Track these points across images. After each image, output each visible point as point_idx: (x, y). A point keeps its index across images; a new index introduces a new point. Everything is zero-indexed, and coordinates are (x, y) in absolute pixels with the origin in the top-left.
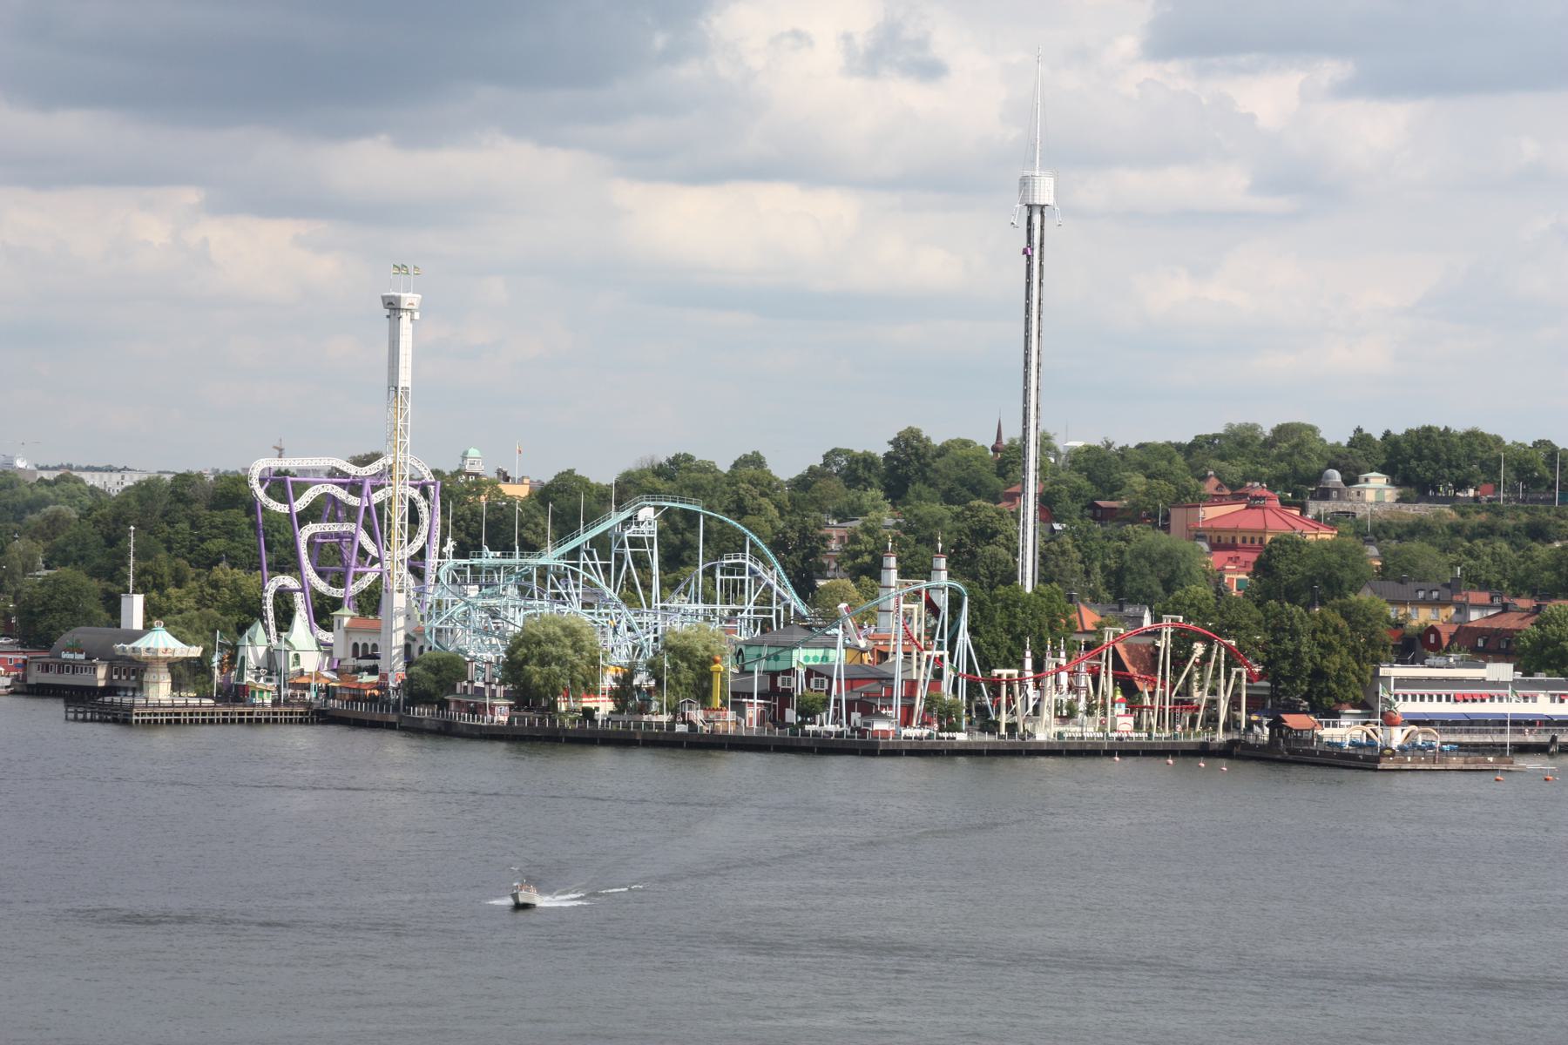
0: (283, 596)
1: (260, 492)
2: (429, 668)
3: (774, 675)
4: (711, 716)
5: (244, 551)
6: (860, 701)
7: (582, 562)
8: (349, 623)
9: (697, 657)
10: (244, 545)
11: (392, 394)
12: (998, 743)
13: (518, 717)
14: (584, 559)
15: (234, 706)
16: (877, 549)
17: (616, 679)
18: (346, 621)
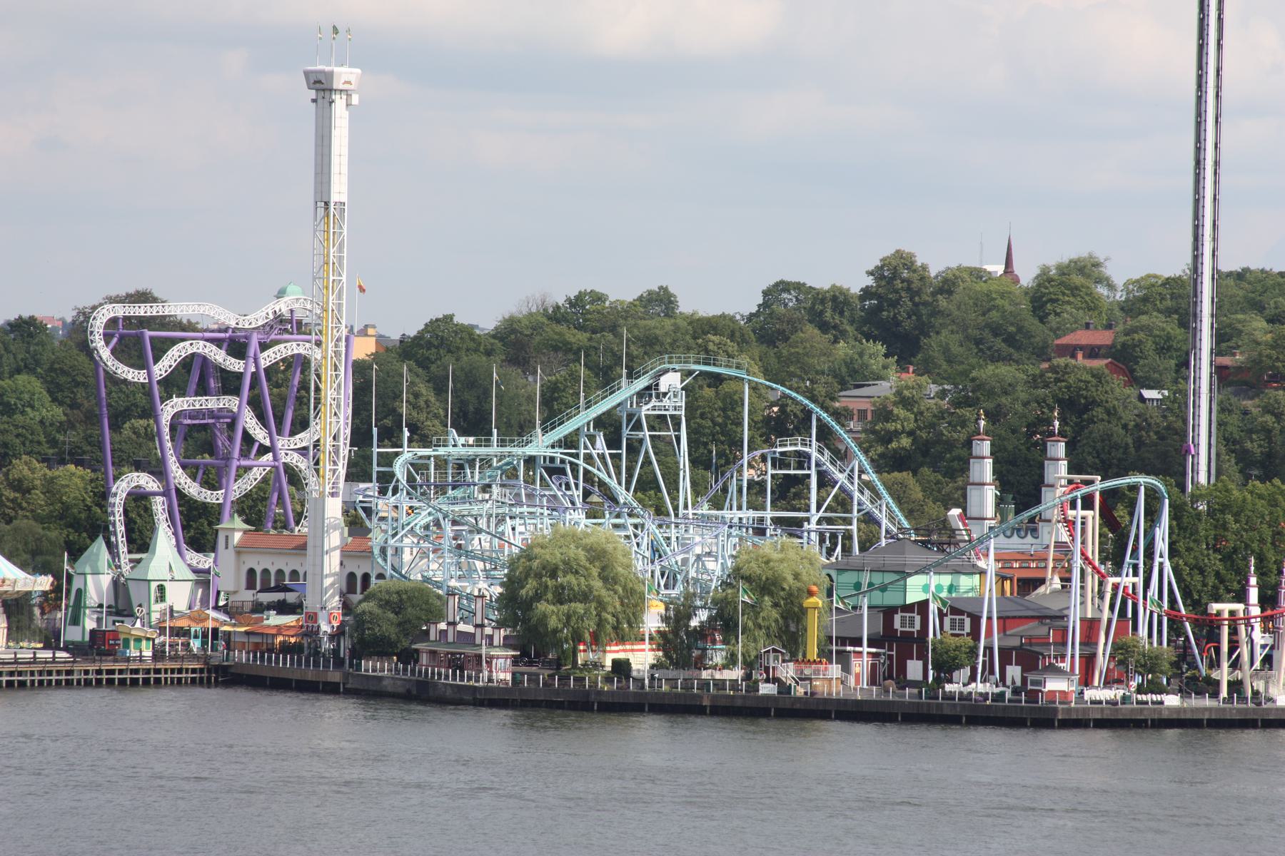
0: (139, 499)
1: (105, 353)
2: (386, 604)
3: (889, 612)
4: (807, 672)
5: (18, 436)
6: (1019, 649)
7: (583, 451)
8: (241, 540)
9: (783, 589)
10: (16, 427)
11: (321, 212)
12: (1224, 709)
13: (529, 674)
14: (586, 447)
15: (101, 661)
16: (919, 428)
17: (665, 619)
18: (237, 536)
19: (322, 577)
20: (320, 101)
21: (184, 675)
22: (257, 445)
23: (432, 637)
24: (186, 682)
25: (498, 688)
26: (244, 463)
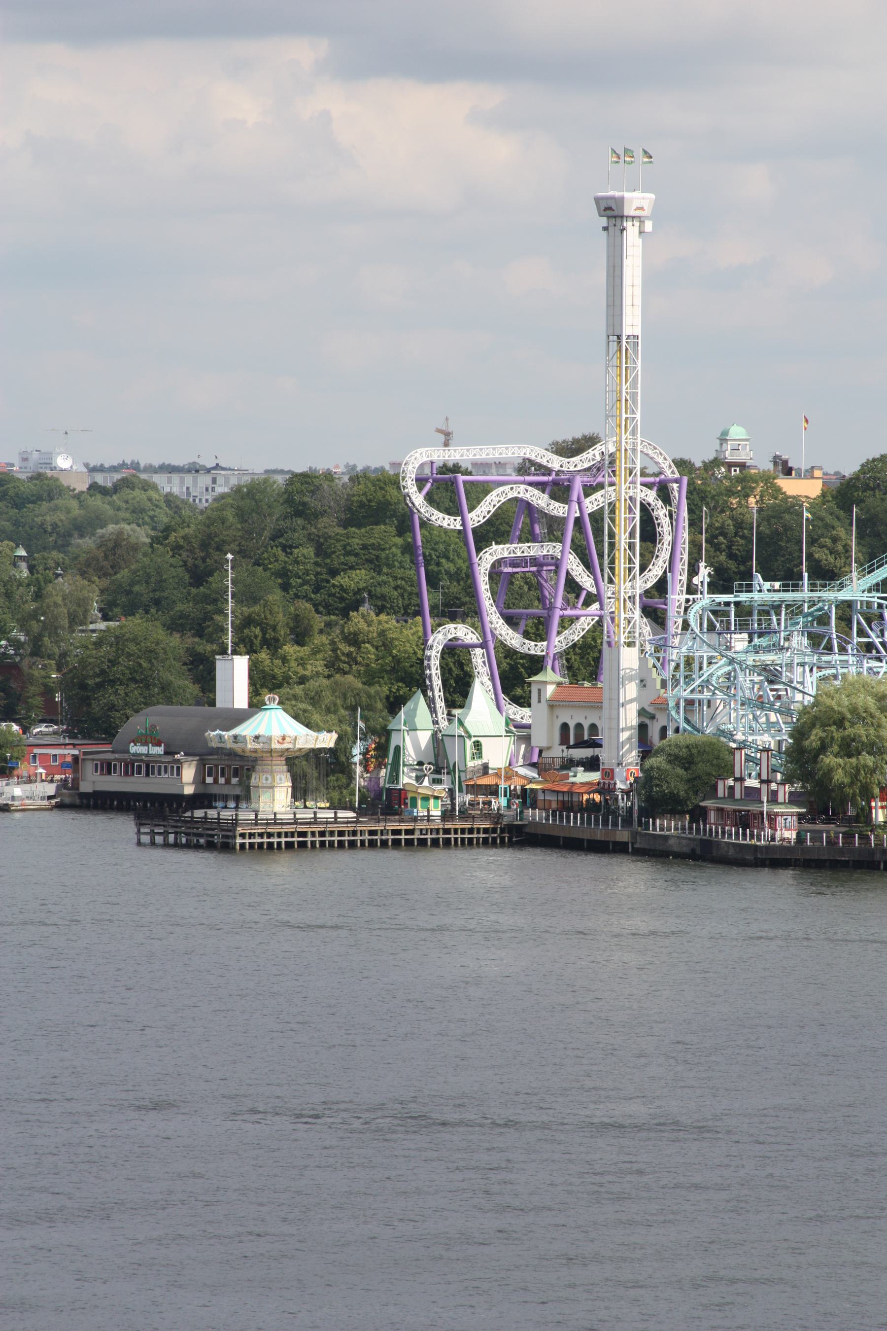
1: (418, 499)
2: (674, 759)
8: (555, 693)
10: (396, 578)
11: (614, 346)
18: (550, 690)
19: (619, 731)
20: (611, 229)
21: (475, 835)
23: (720, 793)
24: (478, 843)
25: (781, 847)
26: (569, 612)
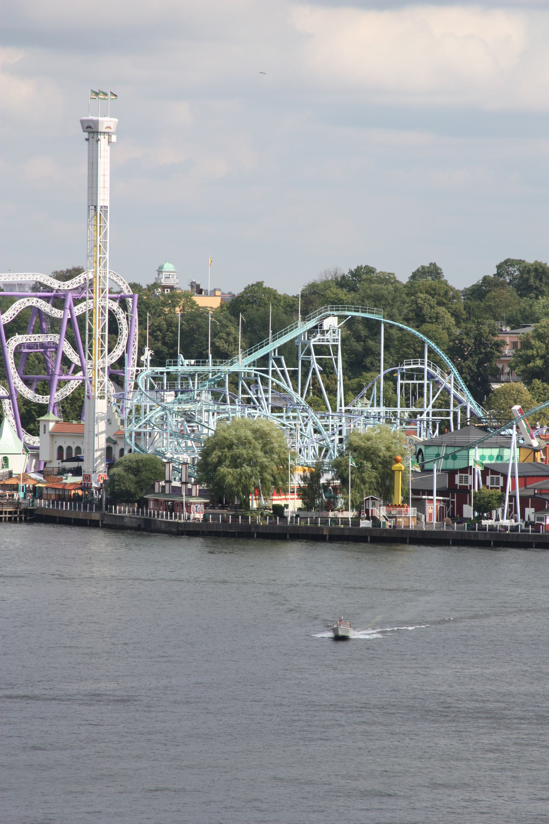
2: (129, 469)
3: (452, 473)
4: (394, 512)
6: (534, 497)
7: (271, 369)
8: (54, 428)
9: (379, 457)
11: (92, 212)
14: (273, 366)
17: (304, 479)
18: (51, 425)
19: (94, 451)
20: (91, 140)
22: (73, 366)
23: (157, 490)
24: (5, 521)
